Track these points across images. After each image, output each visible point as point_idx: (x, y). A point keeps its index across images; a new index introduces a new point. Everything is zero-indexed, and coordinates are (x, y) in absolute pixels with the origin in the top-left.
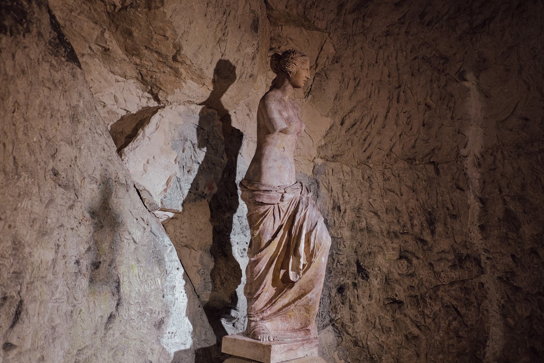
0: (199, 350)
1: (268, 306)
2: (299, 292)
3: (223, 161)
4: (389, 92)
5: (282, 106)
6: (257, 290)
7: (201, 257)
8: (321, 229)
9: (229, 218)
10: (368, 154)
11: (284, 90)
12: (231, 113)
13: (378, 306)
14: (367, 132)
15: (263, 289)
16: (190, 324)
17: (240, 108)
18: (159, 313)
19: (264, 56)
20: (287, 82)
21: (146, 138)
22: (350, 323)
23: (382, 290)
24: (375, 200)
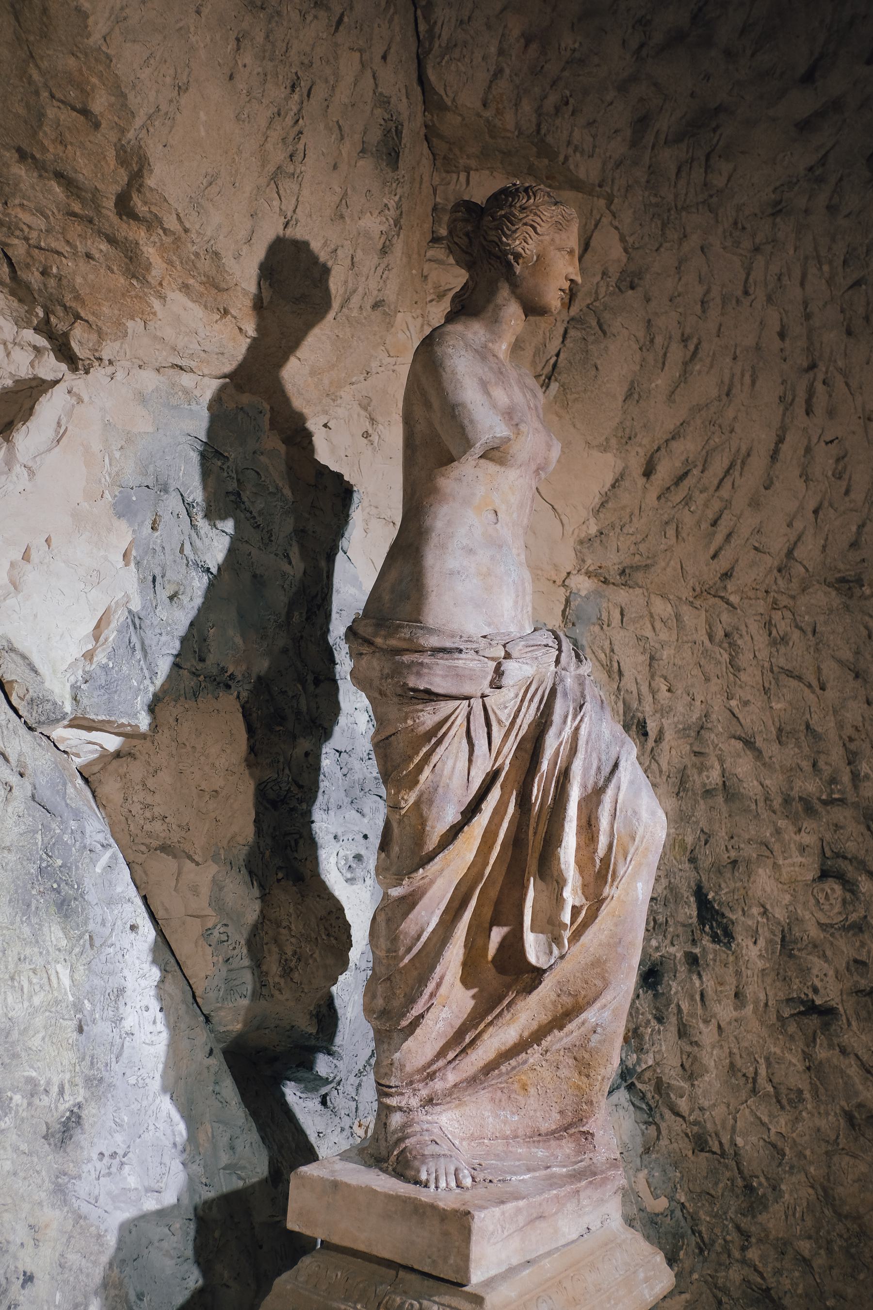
0: (208, 1204)
1: (451, 1055)
2: (554, 1003)
3: (286, 568)
4: (784, 382)
5: (491, 368)
6: (411, 1000)
7: (217, 885)
8: (632, 782)
9: (307, 754)
10: (723, 564)
11: (495, 321)
12: (314, 425)
13: (762, 1023)
14: (721, 499)
15: (432, 995)
16: (176, 1117)
17: (341, 412)
18: (61, 1092)
19: (415, 256)
20: (504, 292)
21: (18, 469)
22: (683, 1078)
23: (773, 974)
24: (746, 703)
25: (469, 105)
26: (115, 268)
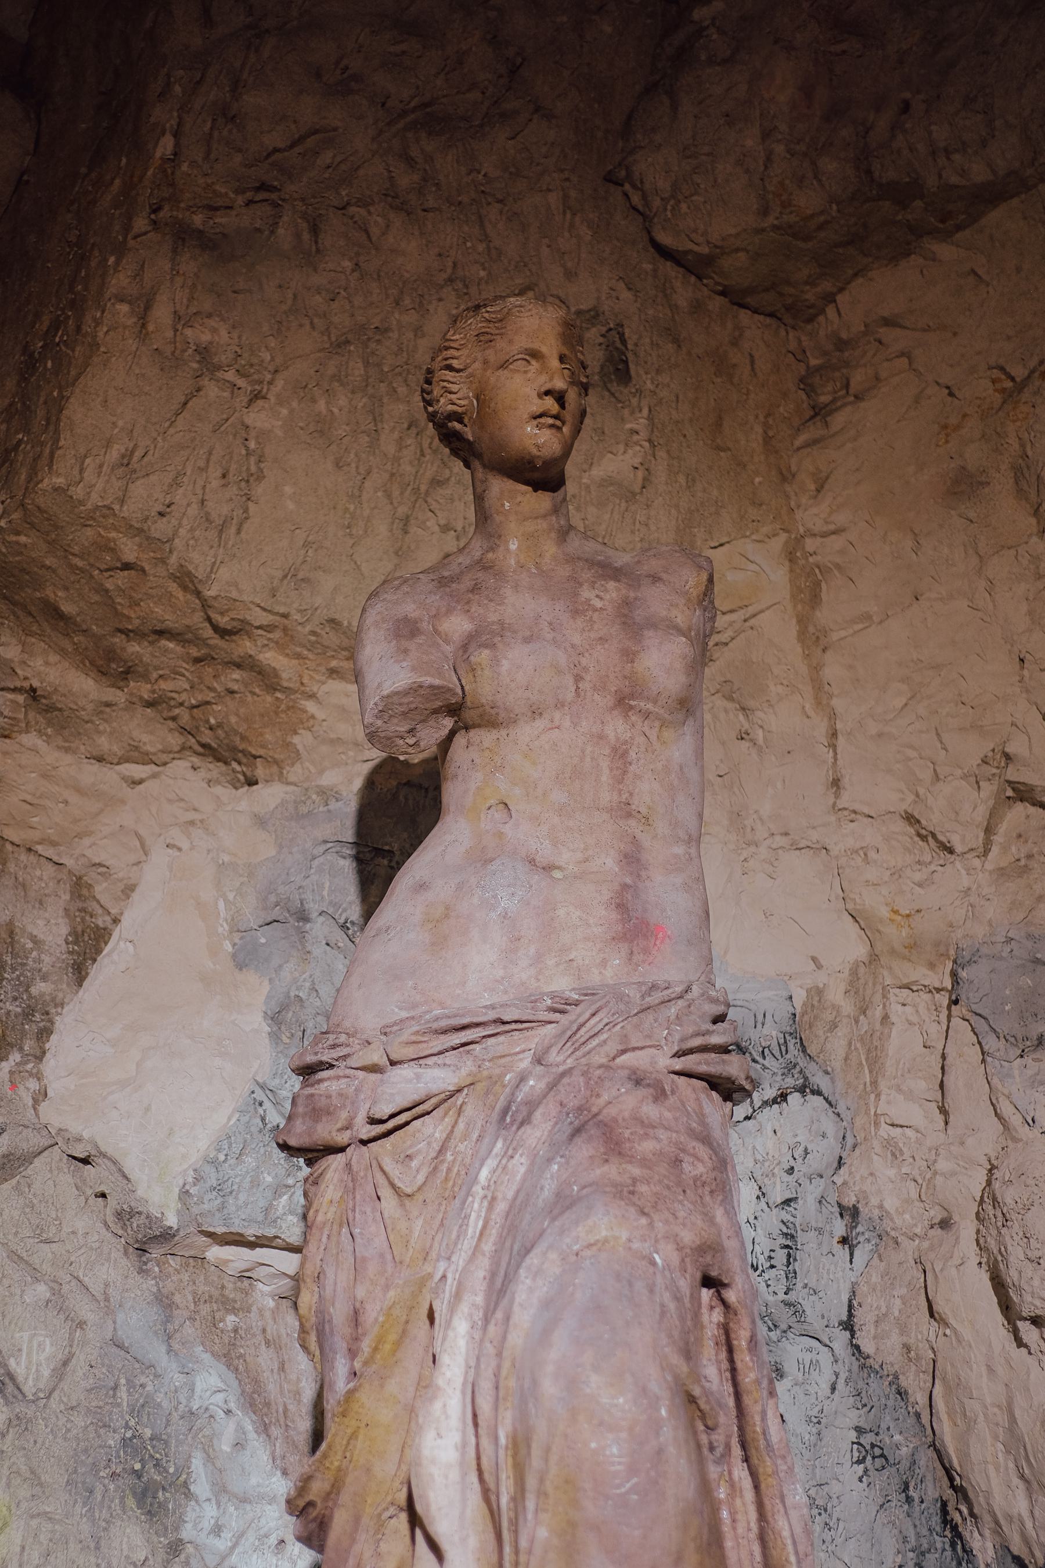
25: (733, 231)
26: (257, 690)
